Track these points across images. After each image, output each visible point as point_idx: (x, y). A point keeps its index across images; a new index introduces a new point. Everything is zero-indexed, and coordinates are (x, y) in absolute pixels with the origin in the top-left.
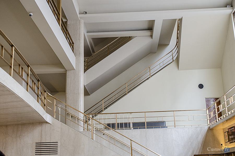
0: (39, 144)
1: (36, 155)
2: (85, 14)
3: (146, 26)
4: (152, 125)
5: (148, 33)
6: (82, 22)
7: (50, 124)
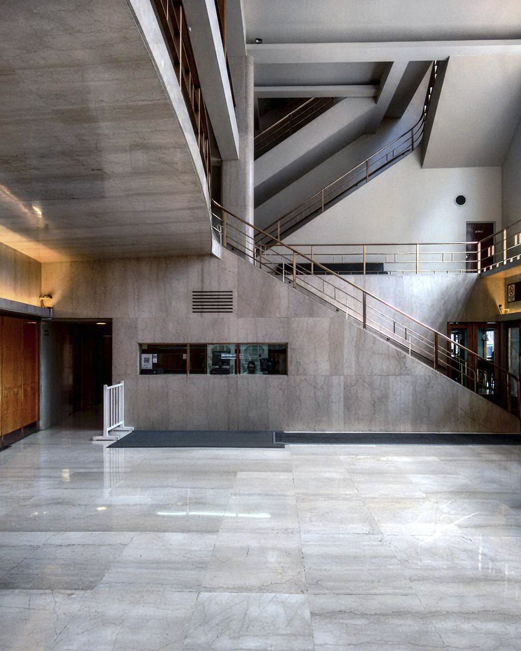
0: (199, 294)
1: (193, 312)
2: (258, 43)
3: (367, 76)
4: (355, 268)
5: (369, 91)
6: (252, 59)
7: (217, 260)
